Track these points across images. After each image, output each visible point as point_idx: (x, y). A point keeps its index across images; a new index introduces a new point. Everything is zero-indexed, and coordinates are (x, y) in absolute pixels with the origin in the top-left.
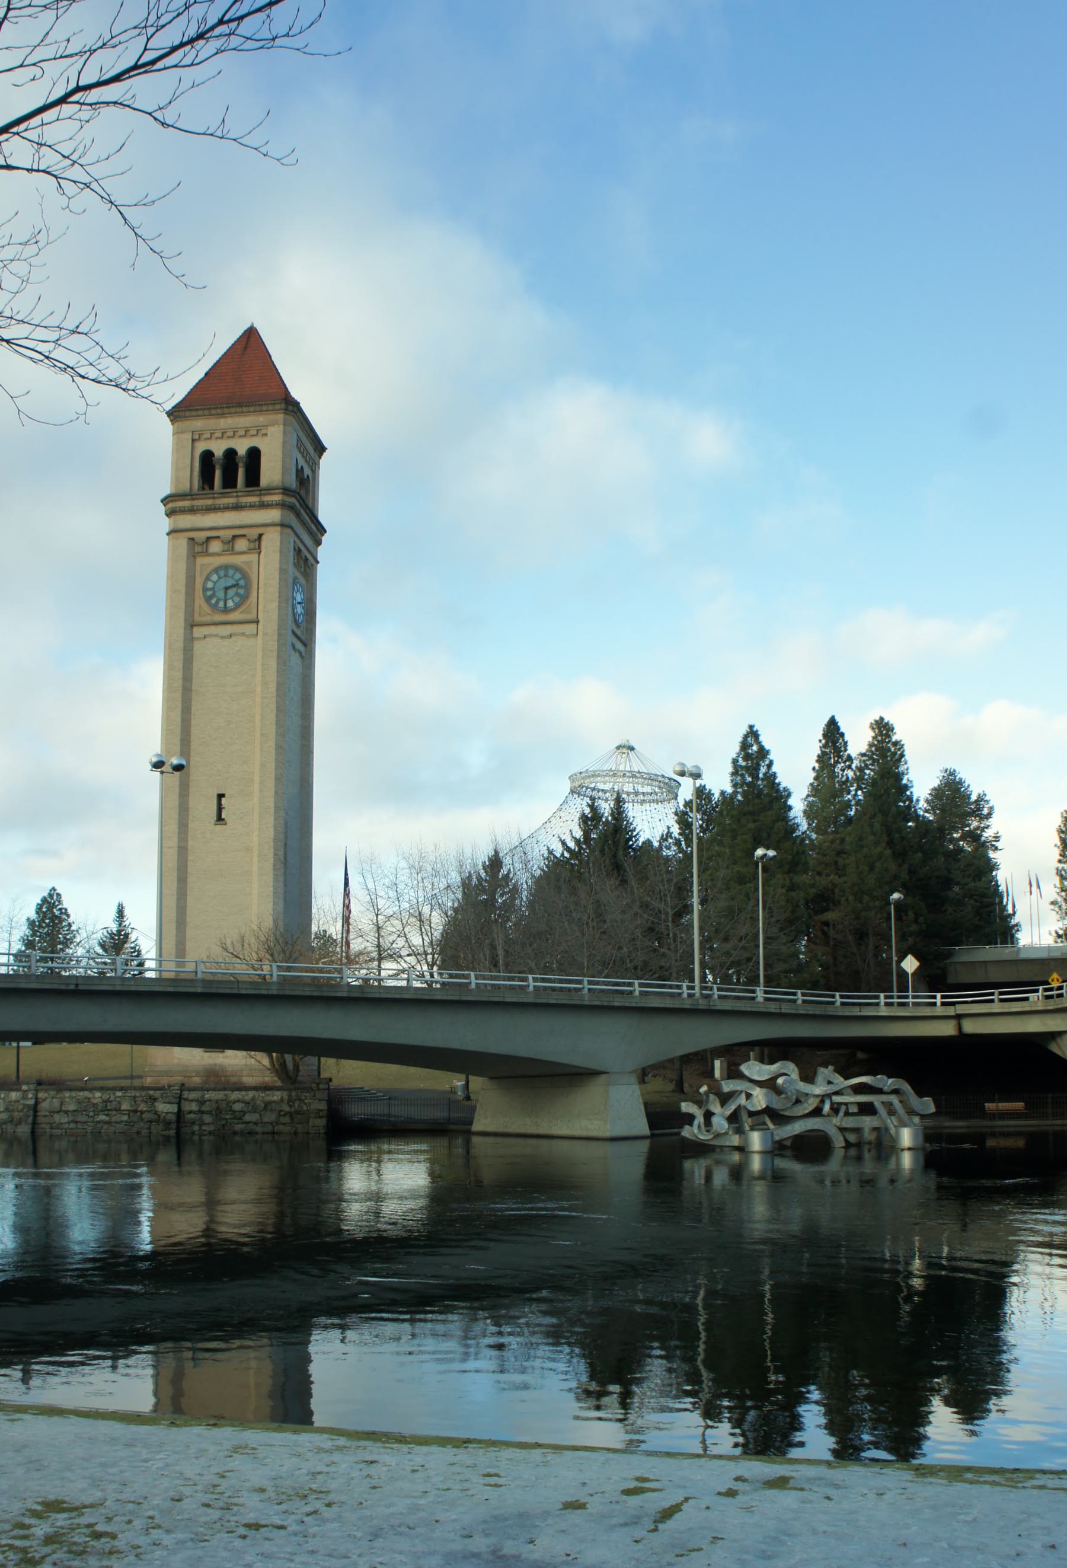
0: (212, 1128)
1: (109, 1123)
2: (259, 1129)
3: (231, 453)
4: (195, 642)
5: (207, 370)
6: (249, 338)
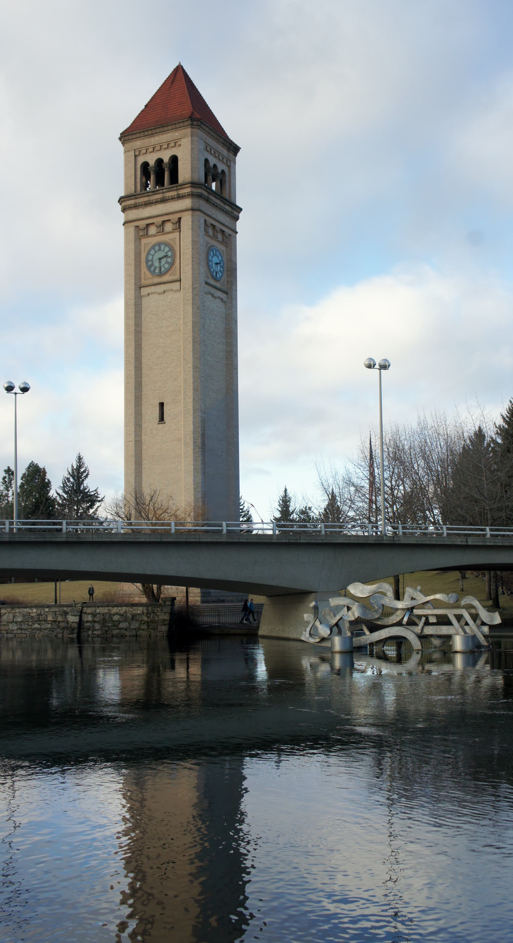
0: (99, 632)
1: (40, 629)
2: (128, 633)
3: (160, 162)
4: (143, 299)
5: (147, 102)
6: (175, 76)
